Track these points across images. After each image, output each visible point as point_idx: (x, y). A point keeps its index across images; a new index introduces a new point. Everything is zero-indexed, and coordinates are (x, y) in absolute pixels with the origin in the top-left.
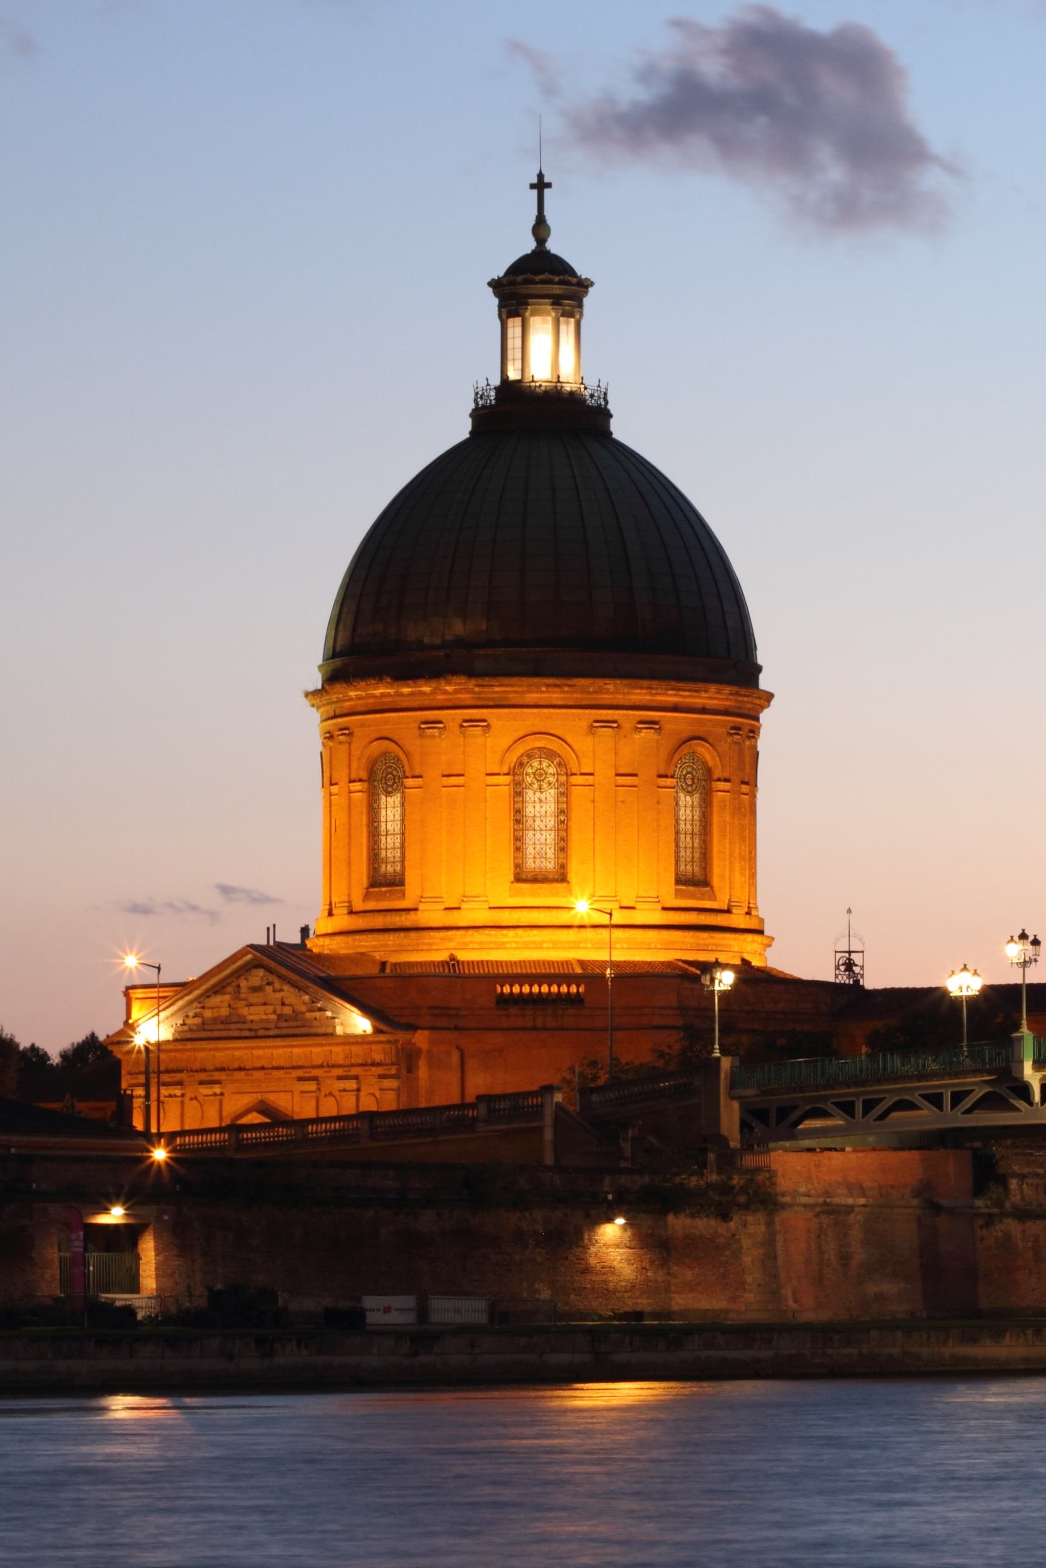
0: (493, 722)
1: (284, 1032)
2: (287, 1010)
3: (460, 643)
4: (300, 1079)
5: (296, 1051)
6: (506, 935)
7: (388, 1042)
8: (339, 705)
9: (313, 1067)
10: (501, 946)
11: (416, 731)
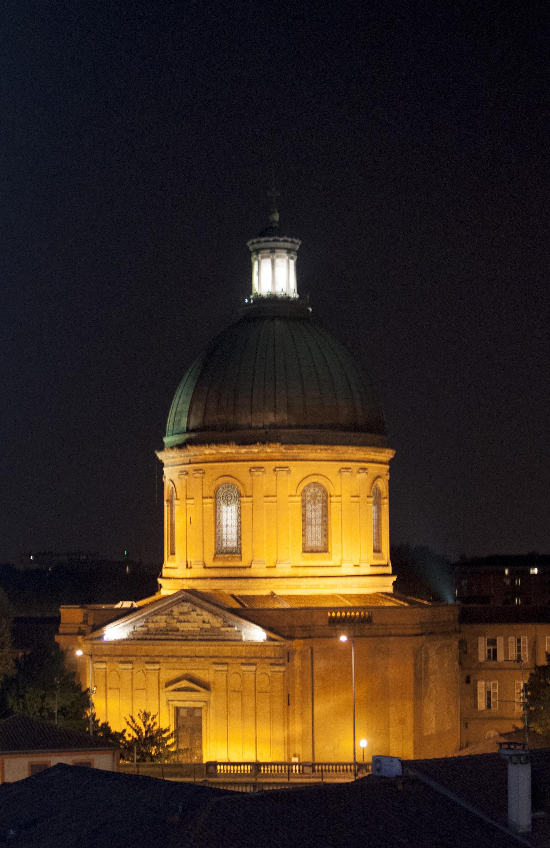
0: (292, 469)
1: (205, 637)
2: (207, 626)
3: (273, 426)
4: (215, 663)
5: (212, 648)
6: (302, 582)
7: (278, 646)
8: (194, 457)
9: (224, 657)
10: (298, 587)
11: (248, 473)
